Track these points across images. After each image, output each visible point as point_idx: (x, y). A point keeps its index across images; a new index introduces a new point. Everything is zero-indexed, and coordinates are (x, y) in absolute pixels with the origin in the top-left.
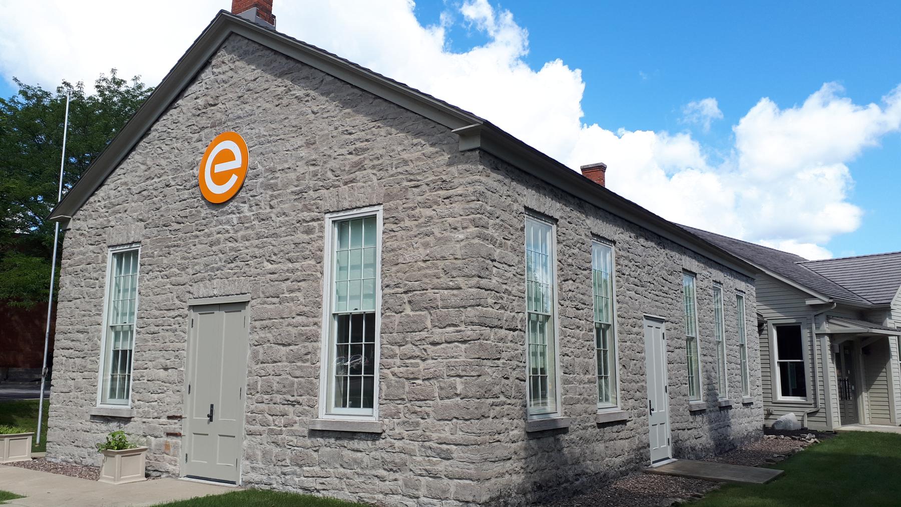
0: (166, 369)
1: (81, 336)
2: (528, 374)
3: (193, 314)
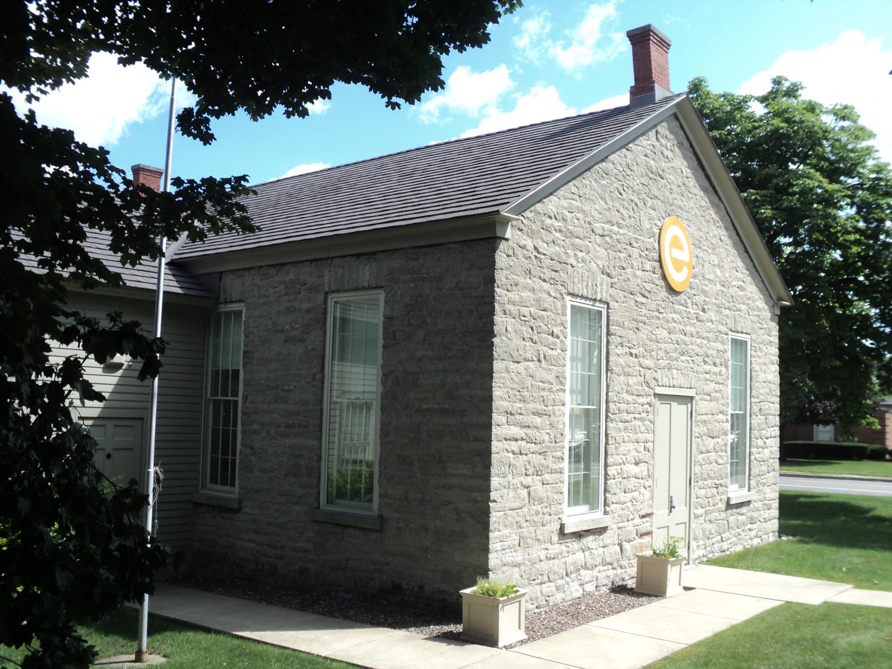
0: (637, 464)
1: (538, 420)
2: (729, 418)
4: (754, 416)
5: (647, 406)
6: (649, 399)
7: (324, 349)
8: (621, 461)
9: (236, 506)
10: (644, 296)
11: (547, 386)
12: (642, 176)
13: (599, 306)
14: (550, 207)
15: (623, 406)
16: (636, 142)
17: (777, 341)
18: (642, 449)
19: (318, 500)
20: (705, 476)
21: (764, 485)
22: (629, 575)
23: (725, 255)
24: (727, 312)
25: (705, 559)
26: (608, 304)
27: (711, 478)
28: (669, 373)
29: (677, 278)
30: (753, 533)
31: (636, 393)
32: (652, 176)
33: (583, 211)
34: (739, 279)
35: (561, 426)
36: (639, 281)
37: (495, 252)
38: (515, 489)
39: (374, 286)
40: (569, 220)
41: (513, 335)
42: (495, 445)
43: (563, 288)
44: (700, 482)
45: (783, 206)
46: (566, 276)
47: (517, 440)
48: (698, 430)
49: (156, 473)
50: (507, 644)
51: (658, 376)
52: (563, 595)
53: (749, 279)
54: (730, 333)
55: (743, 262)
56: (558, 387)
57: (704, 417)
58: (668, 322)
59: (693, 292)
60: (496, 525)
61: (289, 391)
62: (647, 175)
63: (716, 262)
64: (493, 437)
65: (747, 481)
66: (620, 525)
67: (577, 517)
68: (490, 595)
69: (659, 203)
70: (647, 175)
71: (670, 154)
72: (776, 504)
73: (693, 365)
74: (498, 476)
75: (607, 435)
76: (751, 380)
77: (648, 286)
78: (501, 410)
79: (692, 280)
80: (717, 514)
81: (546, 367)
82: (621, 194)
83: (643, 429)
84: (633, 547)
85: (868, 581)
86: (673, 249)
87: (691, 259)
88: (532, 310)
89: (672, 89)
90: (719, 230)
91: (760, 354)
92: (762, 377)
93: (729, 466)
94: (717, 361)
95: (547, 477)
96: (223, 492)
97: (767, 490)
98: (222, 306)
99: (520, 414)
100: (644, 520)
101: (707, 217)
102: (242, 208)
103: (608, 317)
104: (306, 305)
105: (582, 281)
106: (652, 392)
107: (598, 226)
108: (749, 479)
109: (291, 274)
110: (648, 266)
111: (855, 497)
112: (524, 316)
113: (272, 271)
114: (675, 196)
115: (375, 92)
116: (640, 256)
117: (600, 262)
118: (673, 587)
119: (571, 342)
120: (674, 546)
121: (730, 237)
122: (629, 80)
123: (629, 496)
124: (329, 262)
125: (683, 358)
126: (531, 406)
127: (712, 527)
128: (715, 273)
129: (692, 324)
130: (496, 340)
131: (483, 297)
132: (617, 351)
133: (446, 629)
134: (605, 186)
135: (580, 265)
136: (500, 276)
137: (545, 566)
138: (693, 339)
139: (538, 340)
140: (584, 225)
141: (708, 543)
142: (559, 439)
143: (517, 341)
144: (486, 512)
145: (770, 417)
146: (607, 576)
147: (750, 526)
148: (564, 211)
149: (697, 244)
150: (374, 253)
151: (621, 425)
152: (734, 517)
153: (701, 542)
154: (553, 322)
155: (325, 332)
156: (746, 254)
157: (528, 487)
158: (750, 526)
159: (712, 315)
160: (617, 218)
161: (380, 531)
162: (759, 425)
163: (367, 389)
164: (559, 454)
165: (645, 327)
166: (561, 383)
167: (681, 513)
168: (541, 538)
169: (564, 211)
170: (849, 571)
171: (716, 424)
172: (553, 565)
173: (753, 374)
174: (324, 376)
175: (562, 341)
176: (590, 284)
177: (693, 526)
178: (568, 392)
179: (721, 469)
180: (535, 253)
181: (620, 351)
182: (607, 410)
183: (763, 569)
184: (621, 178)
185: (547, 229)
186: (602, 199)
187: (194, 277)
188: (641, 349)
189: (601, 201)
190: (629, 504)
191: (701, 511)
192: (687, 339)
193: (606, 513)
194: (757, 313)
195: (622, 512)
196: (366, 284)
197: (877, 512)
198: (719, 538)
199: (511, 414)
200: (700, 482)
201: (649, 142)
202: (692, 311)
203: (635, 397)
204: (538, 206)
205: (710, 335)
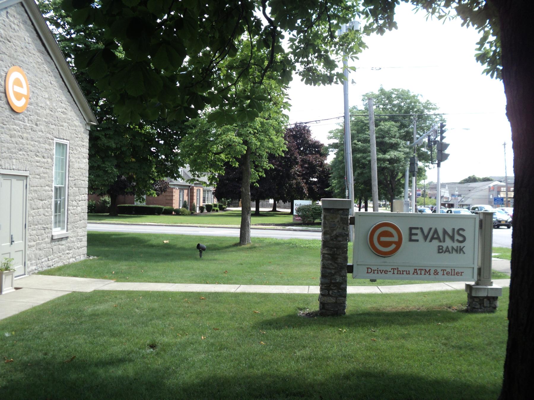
2: (53, 189)
17: (88, 145)
20: (36, 223)
21: (77, 228)
23: (54, 92)
24: (54, 126)
25: (36, 271)
27: (40, 224)
28: (10, 161)
29: (18, 104)
30: (70, 255)
34: (63, 108)
44: (32, 227)
48: (31, 195)
53: (70, 108)
54: (55, 139)
55: (66, 97)
57: (35, 188)
58: (10, 130)
59: (29, 113)
63: (47, 96)
65: (66, 226)
69: (7, 57)
71: (16, 28)
72: (85, 239)
73: (27, 157)
76: (69, 167)
79: (28, 106)
80: (44, 245)
85: (124, 277)
86: (15, 87)
87: (28, 93)
90: (50, 77)
91: (75, 152)
92: (76, 165)
93: (53, 217)
94: (45, 155)
97: (79, 230)
101: (42, 69)
108: (67, 225)
111: (140, 234)
114: (19, 54)
120: (7, 264)
121: (57, 82)
125: (21, 153)
128: (46, 103)
129: (27, 133)
138: (28, 142)
141: (38, 262)
145: (82, 189)
147: (68, 251)
149: (32, 84)
152: (56, 246)
158: (68, 251)
167: (19, 243)
170: (117, 273)
171: (44, 192)
173: (70, 163)
179: (47, 219)
183: (69, 275)
191: (33, 243)
194: (74, 128)
197: (151, 242)
198: (46, 259)
200: (32, 227)
205: (41, 140)
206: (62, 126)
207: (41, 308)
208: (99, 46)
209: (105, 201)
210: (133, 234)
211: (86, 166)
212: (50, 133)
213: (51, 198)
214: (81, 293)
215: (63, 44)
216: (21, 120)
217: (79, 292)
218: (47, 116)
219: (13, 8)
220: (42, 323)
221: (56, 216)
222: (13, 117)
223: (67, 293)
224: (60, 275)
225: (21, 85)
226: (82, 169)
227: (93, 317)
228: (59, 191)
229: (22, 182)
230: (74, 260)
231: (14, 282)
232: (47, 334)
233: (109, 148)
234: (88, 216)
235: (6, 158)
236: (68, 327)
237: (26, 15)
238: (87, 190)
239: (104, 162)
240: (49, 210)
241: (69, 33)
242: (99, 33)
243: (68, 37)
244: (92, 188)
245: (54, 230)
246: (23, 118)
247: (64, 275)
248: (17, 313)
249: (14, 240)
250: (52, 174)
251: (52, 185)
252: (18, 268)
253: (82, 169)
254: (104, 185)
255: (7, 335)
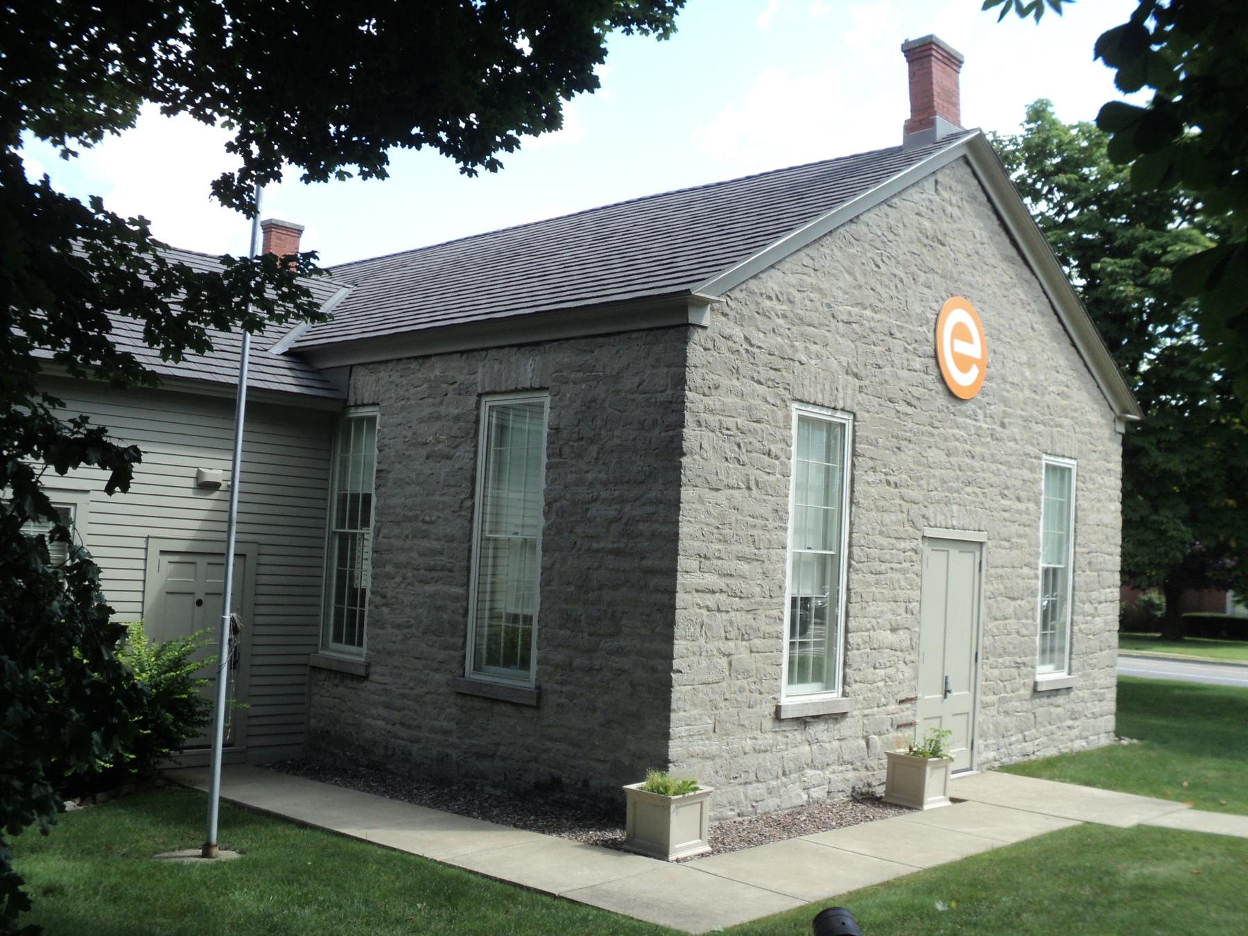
1: (744, 567)
2: (1040, 572)
3: (926, 548)
4: (1079, 572)
5: (912, 553)
6: (914, 544)
7: (475, 469)
8: (869, 626)
9: (362, 672)
10: (909, 404)
11: (759, 522)
12: (912, 242)
13: (840, 417)
14: (770, 284)
15: (875, 553)
16: (904, 196)
18: (902, 611)
19: (462, 664)
21: (1093, 667)
22: (878, 780)
23: (1039, 349)
24: (1040, 428)
25: (997, 764)
26: (854, 415)
27: (1010, 654)
29: (962, 379)
30: (1075, 732)
31: (893, 534)
32: (926, 241)
33: (820, 290)
34: (1061, 383)
35: (780, 576)
36: (903, 384)
37: (686, 343)
38: (710, 657)
39: (537, 386)
40: (798, 303)
41: (711, 454)
42: (681, 598)
43: (787, 393)
44: (992, 659)
45: (1153, 281)
46: (791, 376)
47: (713, 592)
49: (233, 620)
50: (681, 855)
51: (930, 512)
52: (777, 801)
54: (1044, 456)
55: (1067, 359)
56: (776, 525)
57: (1000, 571)
58: (946, 439)
59: (986, 399)
60: (680, 704)
61: (431, 523)
62: (919, 240)
63: (1024, 359)
64: (679, 588)
65: (1067, 660)
66: (867, 712)
67: (799, 697)
68: (659, 792)
69: (937, 278)
70: (919, 240)
71: (956, 212)
72: (1112, 694)
74: (685, 638)
75: (848, 589)
76: (1076, 522)
77: (917, 392)
78: (690, 552)
79: (985, 383)
80: (1017, 704)
81: (758, 497)
82: (878, 267)
83: (903, 583)
84: (885, 744)
85: (1214, 800)
86: (956, 341)
88: (739, 421)
89: (963, 124)
90: (1030, 315)
91: (1091, 486)
92: (1093, 518)
93: (1038, 639)
94: (1023, 494)
95: (757, 642)
96: (349, 653)
97: (1096, 673)
98: (353, 410)
99: (719, 558)
100: (903, 706)
101: (1012, 298)
102: (307, 293)
103: (854, 431)
104: (454, 411)
105: (816, 383)
106: (919, 535)
107: (842, 310)
108: (1070, 659)
109: (436, 370)
110: (917, 363)
112: (728, 429)
113: (414, 365)
114: (961, 268)
115: (448, 156)
116: (906, 350)
117: (842, 358)
118: (934, 800)
119: (800, 466)
120: (937, 742)
122: (904, 111)
123: (881, 672)
124: (484, 353)
125: (968, 489)
126: (735, 548)
127: (1010, 722)
128: (1022, 374)
129: (983, 444)
130: (685, 461)
131: (671, 402)
132: (866, 477)
133: (609, 835)
134: (854, 256)
135: (813, 362)
136: (694, 376)
137: (751, 761)
138: (985, 465)
139: (747, 461)
140: (821, 309)
141: (1002, 742)
142: (776, 592)
143: (715, 462)
144: (666, 687)
145: (1105, 574)
146: (845, 779)
147: (1070, 723)
148: (791, 290)
149: (992, 334)
150: (538, 344)
151: (871, 578)
152: (1043, 708)
153: (991, 741)
154: (771, 438)
155: (476, 446)
156: (1072, 349)
157: (729, 655)
158: (1070, 723)
159: (1016, 431)
160: (872, 298)
161: (537, 707)
162: (1086, 583)
163: (529, 521)
164: (775, 613)
165: (911, 446)
166: (781, 519)
168: (746, 723)
169: (791, 290)
170: (1193, 787)
171: (1019, 580)
172: (764, 760)
173: (1079, 513)
174: (473, 504)
175: (783, 464)
176: (827, 387)
177: (979, 718)
178: (790, 532)
180: (746, 346)
181: (871, 477)
182: (850, 557)
183: (1074, 780)
184: (879, 245)
185: (764, 314)
186: (849, 272)
187: (319, 371)
188: (904, 476)
189: (847, 276)
190: (881, 684)
191: (991, 698)
192: (976, 464)
193: (844, 694)
194: (1087, 430)
195: (869, 694)
196: (527, 385)
198: (1020, 736)
199: (706, 557)
200: (992, 659)
201: (924, 196)
202: (985, 426)
203: (894, 541)
204: (753, 284)
205: (1013, 459)
206: (1060, 426)
207: (1014, 854)
208: (1137, 234)
209: (1150, 605)
210: (1227, 689)
211: (1115, 518)
212: (1032, 444)
213: (1033, 594)
214: (1105, 828)
215: (1052, 236)
216: (969, 417)
217: (1099, 825)
218: (1025, 404)
219: (948, 171)
220: (1017, 890)
221: (1044, 635)
222: (952, 409)
223: (1072, 823)
224: (1052, 778)
225: (969, 339)
226: (1106, 526)
227: (1141, 893)
228: (1052, 577)
229: (971, 555)
230: (1084, 744)
231: (949, 784)
232: (1031, 919)
233: (1169, 475)
234: (1121, 638)
235: (938, 502)
236: (1080, 909)
237: (976, 182)
238: (1117, 576)
239: (1155, 510)
240: (1030, 621)
241: (1062, 210)
242: (1135, 201)
243: (1061, 219)
244: (1131, 575)
245: (1040, 669)
246: (974, 411)
247: (1062, 778)
248: (958, 857)
249: (950, 687)
250: (1038, 538)
251: (1037, 564)
252: (955, 750)
253: (1106, 526)
254: (1158, 566)
255: (940, 906)
